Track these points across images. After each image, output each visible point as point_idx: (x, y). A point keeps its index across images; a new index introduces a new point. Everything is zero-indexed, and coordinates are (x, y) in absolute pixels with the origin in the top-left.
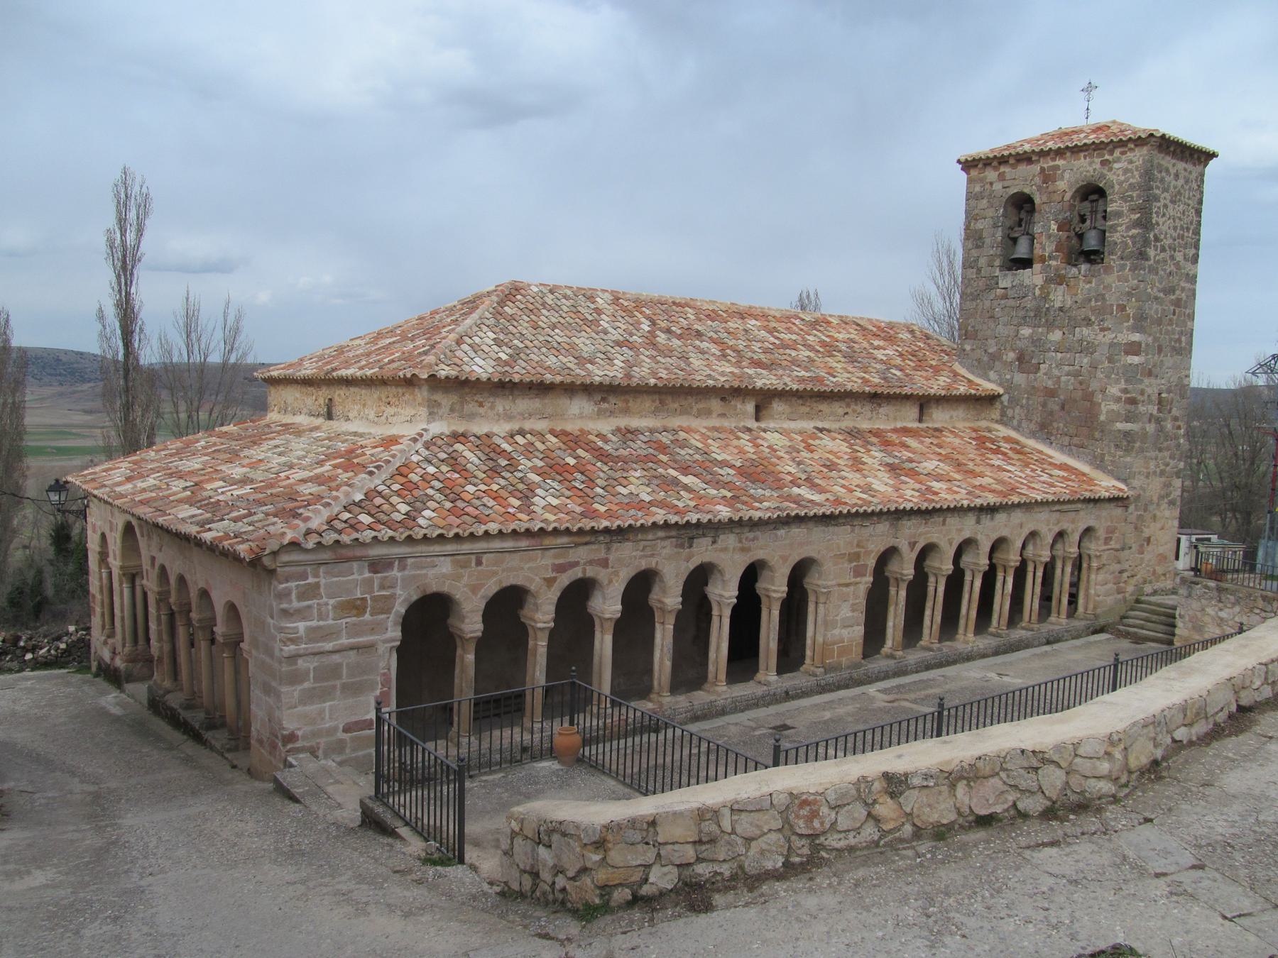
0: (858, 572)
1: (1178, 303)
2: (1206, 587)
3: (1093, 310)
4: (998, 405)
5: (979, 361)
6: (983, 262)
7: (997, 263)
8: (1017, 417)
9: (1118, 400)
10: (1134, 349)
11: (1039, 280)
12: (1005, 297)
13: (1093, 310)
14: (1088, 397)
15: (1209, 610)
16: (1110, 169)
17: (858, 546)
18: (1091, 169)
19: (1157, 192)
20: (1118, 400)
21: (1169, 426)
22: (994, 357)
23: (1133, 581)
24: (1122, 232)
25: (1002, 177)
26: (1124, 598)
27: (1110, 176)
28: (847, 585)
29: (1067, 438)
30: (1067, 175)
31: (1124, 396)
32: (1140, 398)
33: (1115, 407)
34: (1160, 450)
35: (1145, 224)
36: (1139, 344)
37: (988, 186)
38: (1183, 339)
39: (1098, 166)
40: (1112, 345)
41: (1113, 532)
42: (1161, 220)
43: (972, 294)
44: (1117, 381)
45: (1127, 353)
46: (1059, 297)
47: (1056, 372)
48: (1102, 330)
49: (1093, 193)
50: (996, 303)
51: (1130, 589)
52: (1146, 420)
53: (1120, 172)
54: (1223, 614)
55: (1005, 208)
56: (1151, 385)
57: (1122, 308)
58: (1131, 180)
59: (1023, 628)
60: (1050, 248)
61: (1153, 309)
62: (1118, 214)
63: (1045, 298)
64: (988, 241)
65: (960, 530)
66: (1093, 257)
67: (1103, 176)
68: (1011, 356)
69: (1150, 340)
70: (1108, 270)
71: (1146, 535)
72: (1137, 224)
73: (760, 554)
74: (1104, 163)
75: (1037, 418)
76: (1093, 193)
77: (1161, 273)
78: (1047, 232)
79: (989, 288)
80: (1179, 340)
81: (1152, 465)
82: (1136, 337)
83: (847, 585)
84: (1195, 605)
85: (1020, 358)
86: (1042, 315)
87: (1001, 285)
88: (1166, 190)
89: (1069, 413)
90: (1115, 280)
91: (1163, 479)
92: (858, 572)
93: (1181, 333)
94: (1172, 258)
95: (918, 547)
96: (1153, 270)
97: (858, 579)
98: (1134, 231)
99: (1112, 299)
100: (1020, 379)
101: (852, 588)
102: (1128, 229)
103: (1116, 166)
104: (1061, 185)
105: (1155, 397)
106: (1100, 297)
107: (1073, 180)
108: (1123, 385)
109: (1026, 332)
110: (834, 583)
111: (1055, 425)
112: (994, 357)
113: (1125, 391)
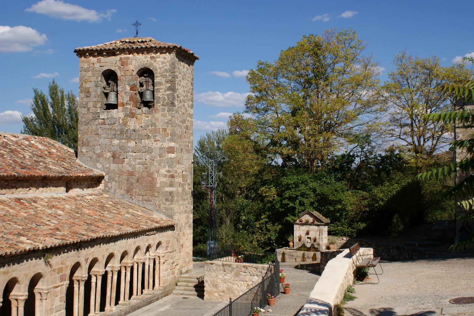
0: (62, 280)
1: (187, 128)
2: (217, 265)
3: (150, 131)
4: (103, 182)
5: (91, 158)
6: (90, 105)
7: (99, 105)
8: (114, 187)
9: (165, 176)
10: (171, 150)
11: (121, 115)
12: (104, 124)
13: (150, 131)
14: (150, 175)
15: (220, 276)
16: (155, 61)
17: (62, 264)
18: (146, 61)
19: (177, 74)
20: (165, 176)
21: (187, 188)
22: (99, 156)
23: (177, 267)
24: (162, 93)
25: (99, 61)
26: (175, 276)
27: (155, 64)
28: (57, 287)
29: (141, 197)
30: (134, 62)
31: (168, 174)
32: (175, 175)
33: (164, 180)
34: (184, 200)
35: (172, 89)
36: (174, 148)
37: (92, 65)
38: (190, 145)
39: (149, 59)
40: (160, 148)
41: (169, 243)
42: (179, 87)
43: (85, 122)
44: (165, 167)
45: (168, 152)
46: (132, 124)
47: (133, 163)
48: (155, 141)
49: (146, 73)
50: (99, 126)
51: (177, 271)
52: (178, 185)
53: (160, 63)
54: (226, 277)
55: (101, 76)
56: (179, 168)
57: (165, 130)
58: (166, 67)
59: (134, 299)
60: (126, 99)
61: (178, 131)
62: (160, 84)
63: (125, 124)
64: (93, 94)
65: (107, 249)
66: (148, 104)
67: (151, 64)
68: (109, 155)
69: (178, 145)
70: (157, 111)
71: (181, 243)
72: (170, 89)
73: (14, 275)
74: (152, 58)
75: (124, 187)
76: (146, 73)
77: (180, 113)
78: (125, 91)
79: (95, 119)
80: (188, 146)
81: (182, 207)
82: (172, 144)
83: (57, 287)
84: (214, 274)
85: (114, 156)
86: (124, 133)
87: (101, 118)
88: (180, 73)
89: (141, 184)
90: (160, 115)
91: (186, 215)
92: (62, 280)
93: (189, 142)
94: (184, 106)
95: (90, 261)
96: (177, 111)
97: (62, 283)
98: (168, 92)
99: (159, 125)
100: (113, 166)
101: (59, 288)
102: (165, 91)
103: (158, 60)
104: (131, 67)
105: (181, 174)
106: (153, 124)
107: (137, 65)
108: (167, 168)
109: (116, 142)
110: (51, 286)
111: (134, 190)
112: (99, 156)
113: (169, 171)
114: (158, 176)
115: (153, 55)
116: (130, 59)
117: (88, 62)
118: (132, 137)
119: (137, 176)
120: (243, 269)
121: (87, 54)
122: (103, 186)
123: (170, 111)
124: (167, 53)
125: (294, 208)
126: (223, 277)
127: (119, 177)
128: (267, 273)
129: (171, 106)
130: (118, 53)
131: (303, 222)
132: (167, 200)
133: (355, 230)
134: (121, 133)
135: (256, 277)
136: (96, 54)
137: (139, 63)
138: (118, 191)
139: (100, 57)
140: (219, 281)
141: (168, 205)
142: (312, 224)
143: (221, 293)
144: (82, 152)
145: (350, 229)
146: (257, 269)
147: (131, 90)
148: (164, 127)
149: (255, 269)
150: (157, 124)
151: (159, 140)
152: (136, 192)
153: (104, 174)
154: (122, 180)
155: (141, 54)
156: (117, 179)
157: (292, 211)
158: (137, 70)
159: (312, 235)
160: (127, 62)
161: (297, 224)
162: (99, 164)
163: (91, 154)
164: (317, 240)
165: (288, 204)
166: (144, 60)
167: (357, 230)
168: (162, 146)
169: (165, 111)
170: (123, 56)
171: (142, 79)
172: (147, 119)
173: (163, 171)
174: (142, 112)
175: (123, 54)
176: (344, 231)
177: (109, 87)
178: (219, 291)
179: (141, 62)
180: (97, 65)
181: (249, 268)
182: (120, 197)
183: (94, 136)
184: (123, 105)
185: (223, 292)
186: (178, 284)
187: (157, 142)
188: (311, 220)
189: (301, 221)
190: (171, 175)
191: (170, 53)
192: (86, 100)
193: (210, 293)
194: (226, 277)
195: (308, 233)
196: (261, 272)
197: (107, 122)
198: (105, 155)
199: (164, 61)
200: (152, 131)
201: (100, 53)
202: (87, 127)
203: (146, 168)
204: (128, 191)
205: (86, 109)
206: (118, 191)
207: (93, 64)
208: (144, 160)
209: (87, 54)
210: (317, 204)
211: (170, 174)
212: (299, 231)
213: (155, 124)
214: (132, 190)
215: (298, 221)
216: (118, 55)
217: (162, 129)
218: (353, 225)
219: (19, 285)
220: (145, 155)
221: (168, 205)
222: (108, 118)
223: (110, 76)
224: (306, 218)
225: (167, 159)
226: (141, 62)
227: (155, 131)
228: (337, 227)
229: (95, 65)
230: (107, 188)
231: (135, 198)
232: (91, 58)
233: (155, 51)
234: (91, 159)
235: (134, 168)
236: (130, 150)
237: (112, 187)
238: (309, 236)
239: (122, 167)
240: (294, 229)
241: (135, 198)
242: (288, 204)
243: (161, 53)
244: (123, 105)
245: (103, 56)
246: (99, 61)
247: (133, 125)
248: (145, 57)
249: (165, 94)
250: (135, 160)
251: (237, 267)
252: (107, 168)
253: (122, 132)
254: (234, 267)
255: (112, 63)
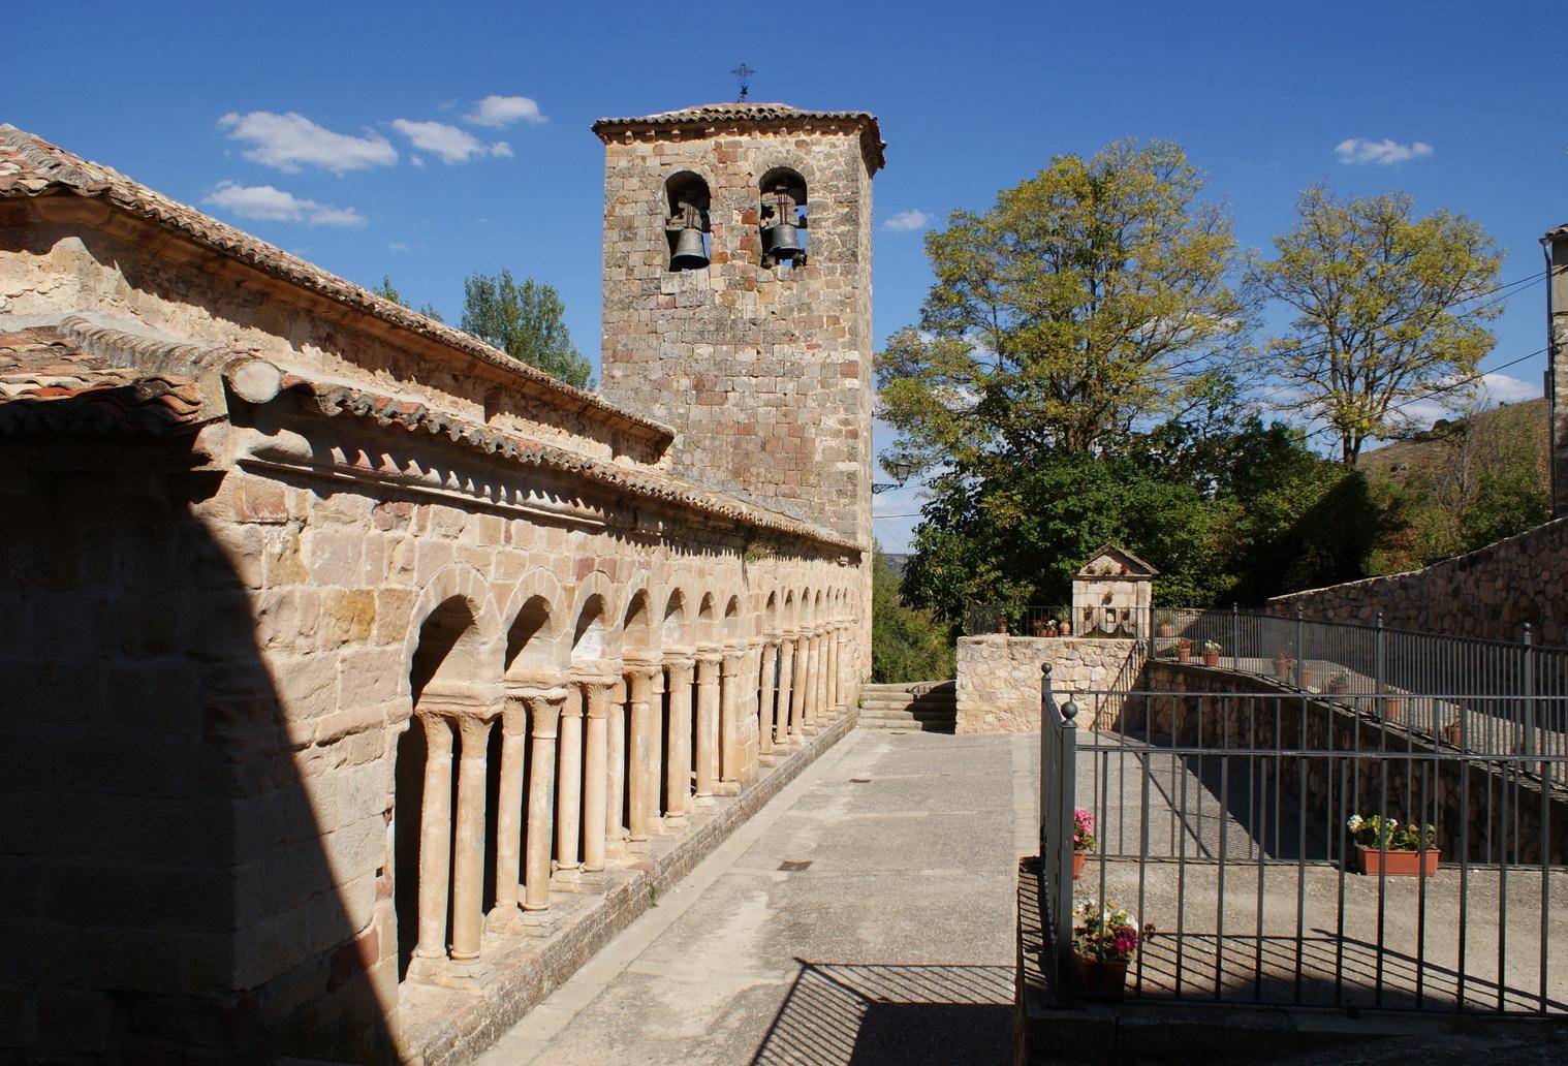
3: (796, 323)
4: (669, 450)
5: (636, 391)
6: (635, 259)
7: (658, 260)
8: (698, 464)
9: (837, 434)
11: (719, 284)
13: (796, 323)
14: (798, 432)
16: (808, 153)
18: (784, 150)
22: (659, 386)
24: (826, 227)
27: (808, 159)
29: (772, 487)
30: (752, 154)
33: (833, 443)
37: (639, 161)
39: (793, 147)
40: (823, 366)
43: (621, 301)
44: (835, 410)
45: (845, 375)
46: (749, 306)
47: (750, 402)
48: (810, 347)
49: (786, 182)
50: (657, 313)
53: (822, 157)
57: (835, 320)
60: (733, 244)
62: (823, 207)
63: (730, 307)
64: (642, 232)
67: (799, 160)
68: (685, 383)
74: (798, 144)
75: (727, 463)
76: (786, 182)
79: (647, 294)
84: (982, 668)
85: (699, 386)
86: (725, 328)
87: (664, 290)
89: (772, 454)
99: (821, 309)
100: (697, 412)
103: (815, 148)
104: (745, 166)
106: (805, 307)
107: (760, 160)
108: (842, 415)
109: (704, 350)
111: (754, 470)
112: (659, 386)
113: (846, 422)
114: (817, 435)
115: (803, 137)
116: (741, 147)
117: (629, 153)
118: (747, 339)
119: (761, 434)
120: (1065, 652)
121: (629, 133)
122: (669, 462)
123: (848, 273)
124: (841, 134)
125: (1075, 540)
126: (1010, 673)
127: (713, 438)
128: (1130, 657)
129: (850, 261)
130: (712, 129)
131: (1096, 574)
132: (840, 492)
133: (1212, 593)
134: (717, 330)
135: (1100, 668)
136: (653, 133)
137: (768, 155)
138: (709, 472)
139: (661, 142)
140: (996, 683)
141: (845, 505)
142: (1121, 577)
143: (1003, 714)
144: (613, 377)
145: (1200, 591)
146: (1103, 648)
147: (745, 221)
148: (832, 313)
149: (1098, 651)
150: (814, 306)
151: (820, 346)
152: (758, 475)
153: (675, 431)
154: (721, 446)
155: (771, 135)
156: (707, 443)
157: (1072, 549)
158: (762, 174)
159: (1119, 602)
160: (736, 153)
161: (1082, 579)
162: (658, 405)
163: (635, 381)
164: (1132, 616)
165: (1063, 531)
166: (780, 149)
167: (1218, 593)
168: (828, 361)
169: (835, 273)
170: (723, 138)
171: (770, 198)
172: (789, 292)
173: (831, 422)
174: (775, 275)
175: (723, 134)
176: (1186, 596)
177: (681, 217)
178: (999, 708)
179: (771, 154)
180: (653, 163)
181: (1082, 649)
182: (716, 489)
183: (644, 337)
184: (723, 258)
185: (1010, 710)
186: (866, 704)
187: (816, 351)
188: (1116, 567)
189: (1091, 571)
190: (851, 431)
191: (846, 134)
192: (623, 246)
193: (974, 715)
194: (1016, 674)
195: (1108, 599)
196: (1116, 656)
197: (681, 301)
198: (675, 385)
199: (832, 151)
200: (802, 324)
201: (664, 130)
202: (626, 314)
203: (785, 415)
204: (736, 474)
205: (624, 270)
206: (709, 472)
207: (644, 158)
208: (781, 395)
209: (629, 133)
210: (1127, 531)
211: (850, 428)
212: (1085, 595)
213: (809, 305)
214: (748, 470)
215: (1083, 572)
216: (711, 135)
217: (828, 317)
218: (1207, 580)
219: (708, 621)
220: (783, 382)
221: (845, 505)
222: (682, 292)
223: (688, 192)
224: (1103, 562)
225: (842, 391)
226: (771, 154)
227: (810, 323)
228: (1170, 587)
229: (648, 161)
230: (680, 467)
231: (756, 489)
232: (638, 144)
233: (809, 127)
234: (636, 393)
235: (755, 415)
236: (744, 371)
237: (693, 464)
238: (1110, 606)
239: (722, 413)
240: (1074, 591)
241: (756, 489)
242: (1063, 531)
243: (823, 133)
244: (723, 258)
245: (671, 138)
246: (658, 152)
247: (750, 307)
248: (783, 143)
249: (835, 233)
250: (756, 395)
251: (1049, 647)
252: (681, 416)
253: (720, 326)
254: (1040, 647)
255: (695, 157)
